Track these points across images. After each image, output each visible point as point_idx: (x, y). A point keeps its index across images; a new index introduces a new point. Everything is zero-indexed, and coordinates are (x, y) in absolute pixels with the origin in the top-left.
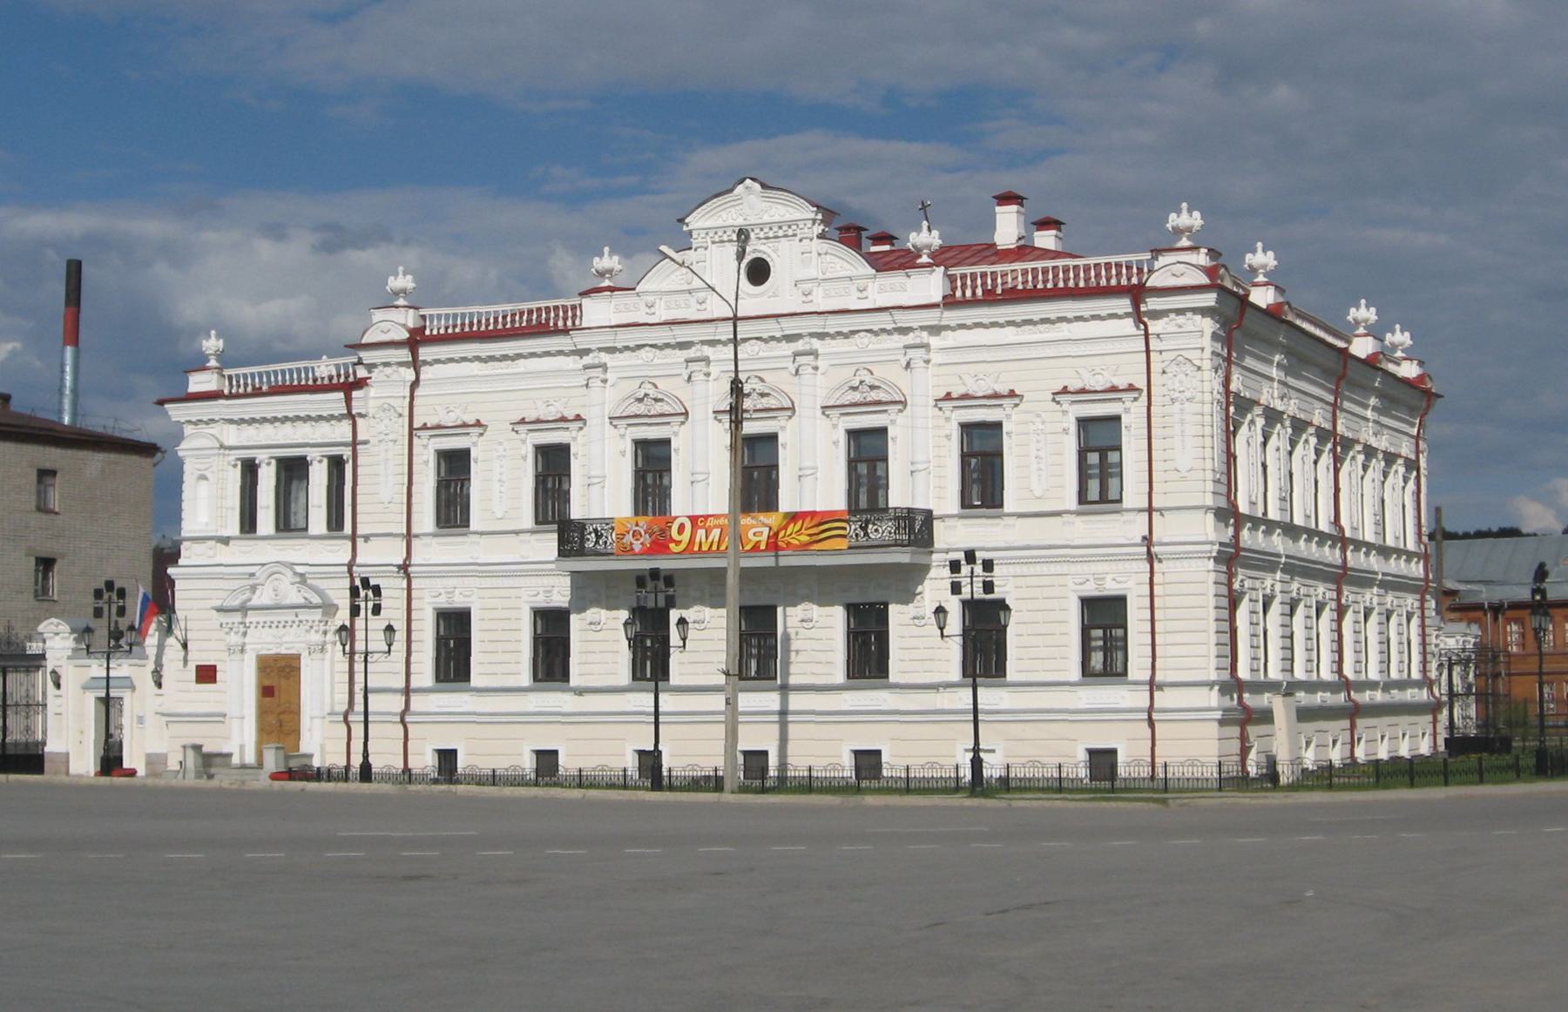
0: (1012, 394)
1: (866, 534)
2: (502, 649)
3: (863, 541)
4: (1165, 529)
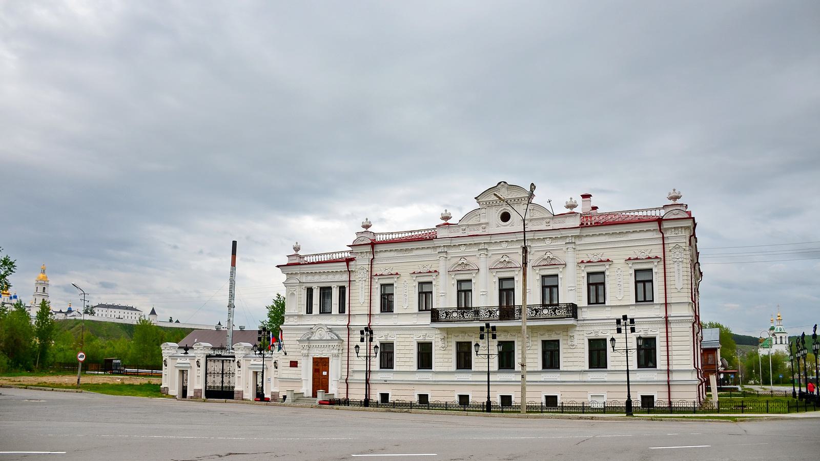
2: (405, 357)
3: (553, 316)
4: (674, 312)
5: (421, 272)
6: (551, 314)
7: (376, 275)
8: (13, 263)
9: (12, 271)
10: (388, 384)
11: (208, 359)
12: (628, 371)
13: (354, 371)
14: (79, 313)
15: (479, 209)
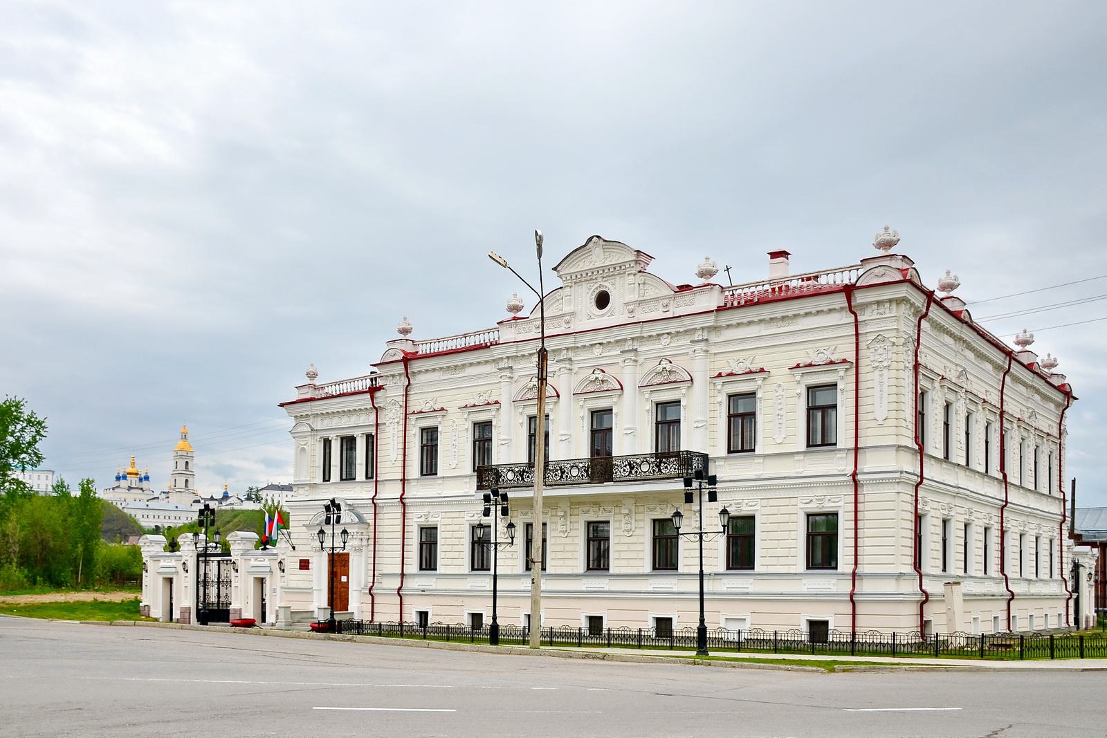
0: (762, 370)
1: (660, 470)
2: (454, 551)
3: (657, 475)
5: (476, 404)
6: (654, 471)
7: (414, 413)
8: (43, 422)
9: (41, 435)
10: (428, 595)
11: (200, 559)
12: (701, 574)
13: (383, 575)
14: (239, 499)
15: (561, 288)
